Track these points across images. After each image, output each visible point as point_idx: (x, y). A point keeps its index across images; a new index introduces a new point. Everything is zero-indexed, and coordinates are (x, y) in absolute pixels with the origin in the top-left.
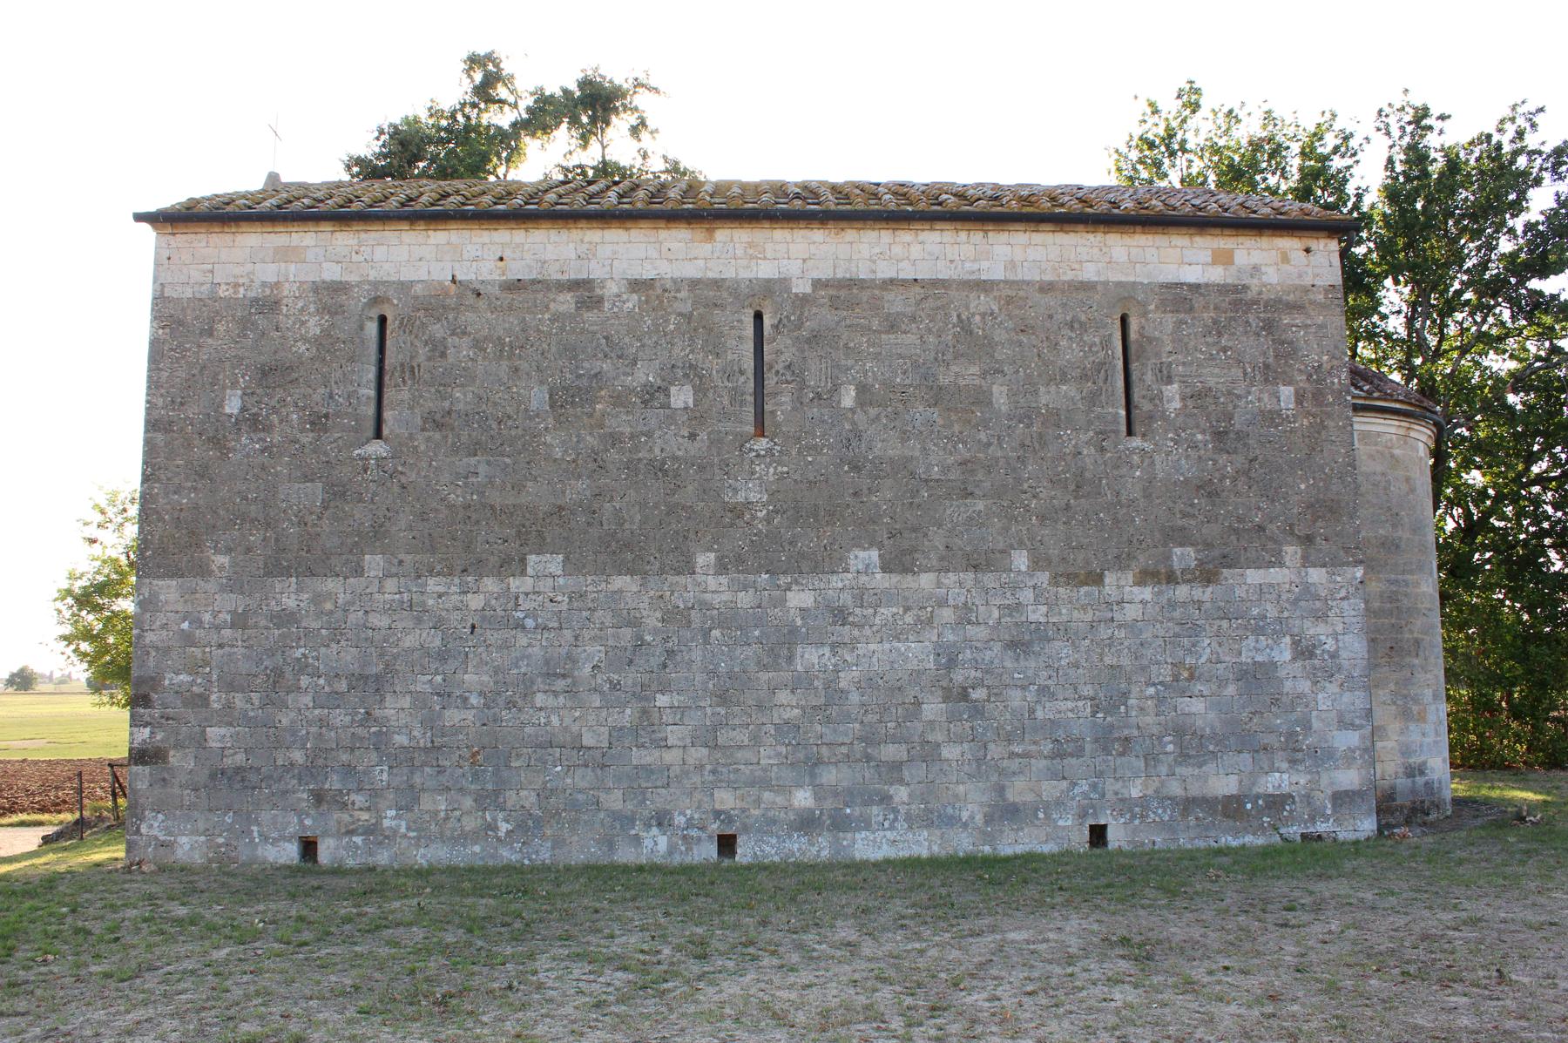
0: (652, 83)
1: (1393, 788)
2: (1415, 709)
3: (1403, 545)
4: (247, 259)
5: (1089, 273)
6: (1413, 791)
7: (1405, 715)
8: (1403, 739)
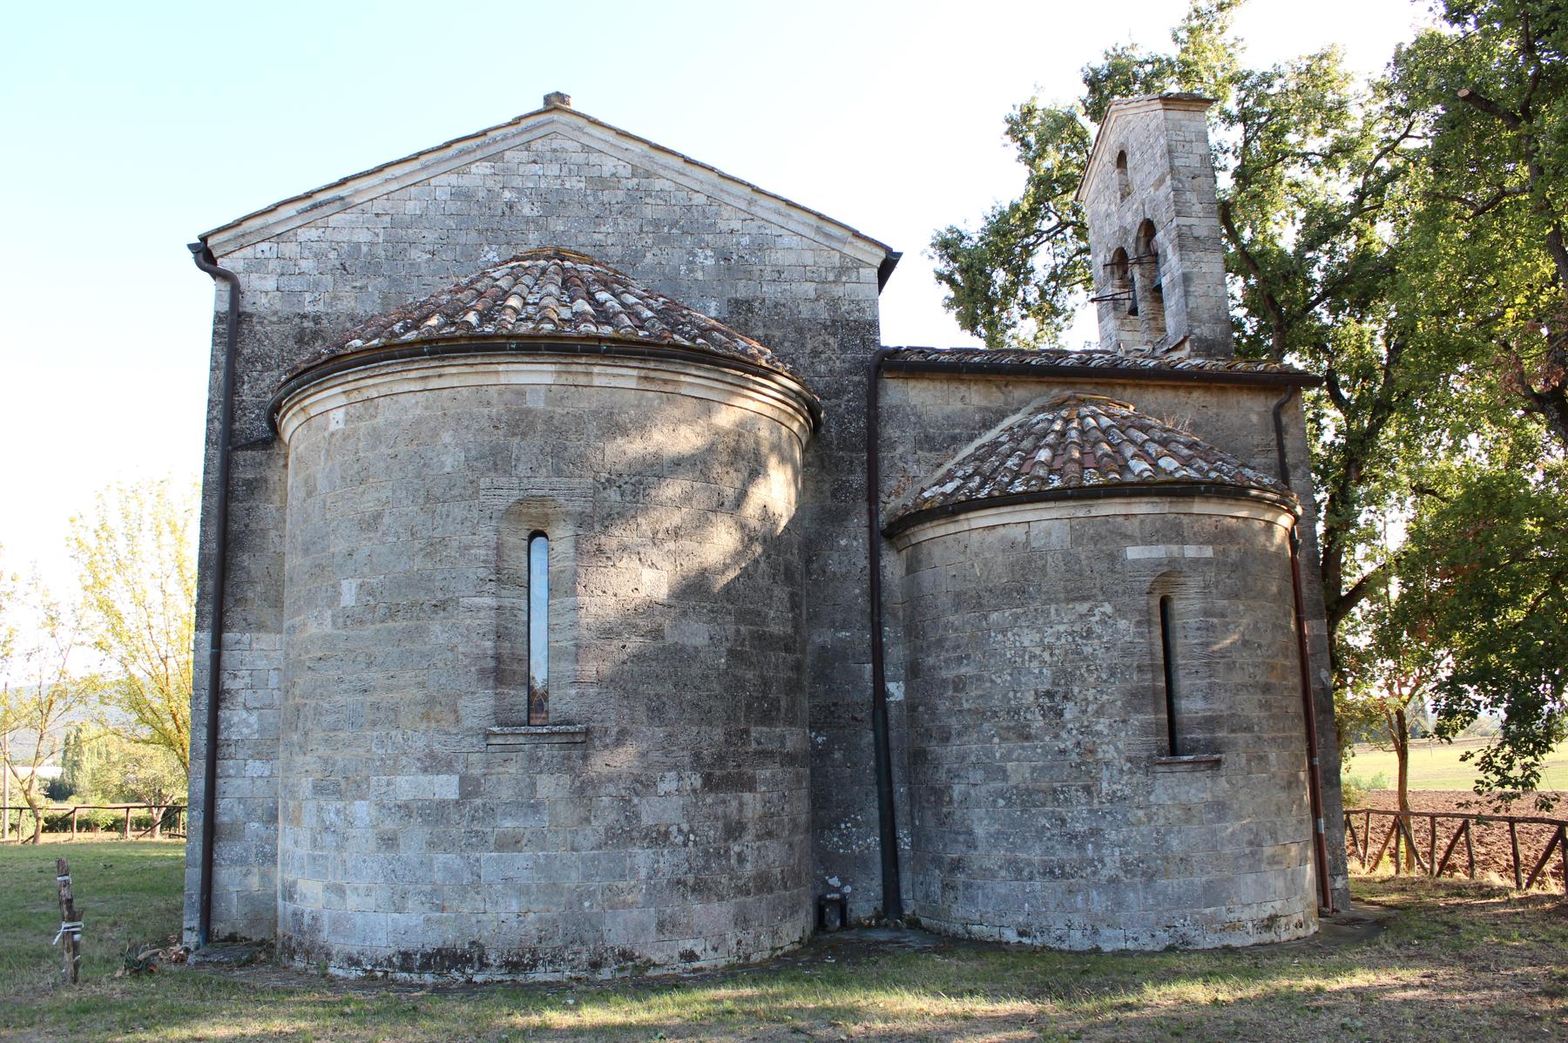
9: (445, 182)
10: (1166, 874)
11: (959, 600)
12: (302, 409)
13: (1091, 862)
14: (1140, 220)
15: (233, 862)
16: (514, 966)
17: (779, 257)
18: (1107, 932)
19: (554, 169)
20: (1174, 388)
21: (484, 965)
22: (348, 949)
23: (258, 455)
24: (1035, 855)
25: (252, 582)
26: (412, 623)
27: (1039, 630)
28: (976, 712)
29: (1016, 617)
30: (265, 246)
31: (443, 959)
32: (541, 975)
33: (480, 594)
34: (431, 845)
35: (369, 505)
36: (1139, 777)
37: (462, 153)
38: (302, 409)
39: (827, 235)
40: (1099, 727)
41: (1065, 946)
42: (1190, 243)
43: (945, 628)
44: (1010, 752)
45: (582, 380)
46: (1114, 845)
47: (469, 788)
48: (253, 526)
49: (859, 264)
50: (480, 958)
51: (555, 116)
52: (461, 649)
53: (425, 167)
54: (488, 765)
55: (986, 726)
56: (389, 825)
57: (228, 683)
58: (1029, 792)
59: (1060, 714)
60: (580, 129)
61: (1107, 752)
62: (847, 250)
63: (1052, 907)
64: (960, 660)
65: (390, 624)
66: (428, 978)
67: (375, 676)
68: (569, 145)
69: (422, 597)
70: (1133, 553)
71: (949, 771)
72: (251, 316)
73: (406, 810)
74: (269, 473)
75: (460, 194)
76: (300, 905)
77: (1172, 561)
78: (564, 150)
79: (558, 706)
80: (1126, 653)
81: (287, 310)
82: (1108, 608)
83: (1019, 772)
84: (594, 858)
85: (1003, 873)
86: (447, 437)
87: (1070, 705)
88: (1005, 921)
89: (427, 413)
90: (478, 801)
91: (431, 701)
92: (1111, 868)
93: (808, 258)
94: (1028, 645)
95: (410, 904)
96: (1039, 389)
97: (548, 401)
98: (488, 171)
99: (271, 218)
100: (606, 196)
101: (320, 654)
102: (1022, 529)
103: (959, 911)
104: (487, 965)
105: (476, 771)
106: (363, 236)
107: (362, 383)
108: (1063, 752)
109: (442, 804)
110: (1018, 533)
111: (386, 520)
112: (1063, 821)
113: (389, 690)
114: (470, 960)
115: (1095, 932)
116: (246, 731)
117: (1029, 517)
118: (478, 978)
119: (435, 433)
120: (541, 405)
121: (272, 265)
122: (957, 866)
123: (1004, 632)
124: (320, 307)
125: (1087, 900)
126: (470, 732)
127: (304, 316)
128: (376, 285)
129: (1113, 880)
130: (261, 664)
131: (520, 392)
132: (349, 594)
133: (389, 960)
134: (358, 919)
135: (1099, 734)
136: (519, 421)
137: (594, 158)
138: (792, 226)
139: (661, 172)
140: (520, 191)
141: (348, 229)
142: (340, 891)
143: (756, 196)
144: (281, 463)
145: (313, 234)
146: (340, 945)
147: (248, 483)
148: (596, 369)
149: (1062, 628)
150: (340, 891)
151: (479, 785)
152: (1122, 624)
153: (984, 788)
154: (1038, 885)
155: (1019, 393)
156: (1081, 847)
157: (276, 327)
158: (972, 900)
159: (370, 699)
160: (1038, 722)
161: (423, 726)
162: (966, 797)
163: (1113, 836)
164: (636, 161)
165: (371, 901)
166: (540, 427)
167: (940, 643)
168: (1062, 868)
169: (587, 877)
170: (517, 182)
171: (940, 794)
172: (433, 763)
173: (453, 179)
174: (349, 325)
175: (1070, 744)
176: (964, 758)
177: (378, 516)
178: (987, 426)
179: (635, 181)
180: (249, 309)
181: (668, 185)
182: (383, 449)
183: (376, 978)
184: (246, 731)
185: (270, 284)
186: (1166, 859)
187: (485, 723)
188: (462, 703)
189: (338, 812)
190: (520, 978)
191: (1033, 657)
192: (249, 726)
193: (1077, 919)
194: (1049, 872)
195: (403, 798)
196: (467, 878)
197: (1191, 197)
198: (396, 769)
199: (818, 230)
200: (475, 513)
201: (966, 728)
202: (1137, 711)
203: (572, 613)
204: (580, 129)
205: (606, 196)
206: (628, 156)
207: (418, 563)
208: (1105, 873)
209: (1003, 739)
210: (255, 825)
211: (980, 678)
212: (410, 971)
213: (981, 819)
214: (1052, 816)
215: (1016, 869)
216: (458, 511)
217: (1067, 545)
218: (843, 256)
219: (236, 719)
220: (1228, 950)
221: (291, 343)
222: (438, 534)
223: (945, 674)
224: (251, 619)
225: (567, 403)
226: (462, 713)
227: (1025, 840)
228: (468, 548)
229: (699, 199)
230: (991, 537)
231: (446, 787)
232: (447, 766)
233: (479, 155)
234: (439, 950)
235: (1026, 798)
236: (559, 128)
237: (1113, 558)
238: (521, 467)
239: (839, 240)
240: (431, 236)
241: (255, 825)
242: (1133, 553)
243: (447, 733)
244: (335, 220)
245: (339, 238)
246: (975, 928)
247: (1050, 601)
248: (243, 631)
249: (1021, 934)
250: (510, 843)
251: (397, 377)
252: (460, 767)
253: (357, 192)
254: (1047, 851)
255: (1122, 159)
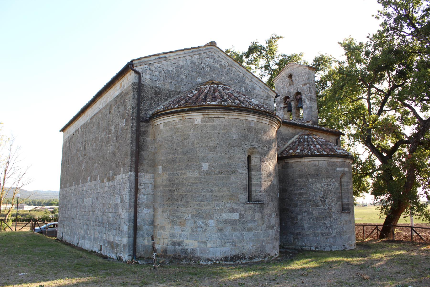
0: (339, 45)
1: (166, 248)
2: (178, 221)
3: (177, 160)
4: (72, 130)
5: (101, 107)
6: (175, 251)
7: (173, 223)
8: (171, 231)
9: (189, 58)
10: (343, 235)
11: (301, 176)
12: (183, 116)
13: (330, 232)
14: (296, 91)
15: (141, 237)
16: (251, 258)
17: (256, 92)
18: (333, 247)
19: (212, 60)
20: (322, 133)
21: (245, 259)
22: (207, 257)
23: (146, 124)
24: (319, 231)
25: (145, 159)
26: (226, 176)
27: (321, 184)
28: (305, 200)
29: (316, 181)
30: (146, 66)
31: (236, 258)
32: (256, 260)
33: (243, 170)
34: (233, 230)
35: (212, 145)
36: (339, 215)
37: (194, 52)
38: (183, 116)
39: (266, 89)
40: (332, 205)
41: (325, 250)
42: (312, 99)
43: (297, 182)
44: (314, 209)
45: (261, 121)
46: (335, 229)
47: (241, 216)
48: (145, 144)
49: (271, 96)
50: (244, 257)
51: (213, 47)
52: (239, 183)
53: (185, 53)
54: (246, 211)
55: (308, 204)
56: (221, 226)
57: (139, 187)
58: (318, 218)
59: (325, 201)
60: (218, 52)
61: (334, 210)
62: (269, 93)
63: (323, 242)
64: (301, 189)
65: (220, 175)
66: (232, 263)
67: (215, 188)
68: (215, 55)
69: (229, 169)
70: (338, 169)
71: (297, 213)
72: (143, 85)
73: (225, 222)
74: (148, 130)
75: (192, 62)
76: (185, 247)
77: (344, 171)
78: (214, 56)
79: (255, 197)
80: (337, 189)
81: (152, 85)
82: (334, 180)
83: (316, 214)
84: (265, 233)
85: (312, 235)
86: (234, 130)
87: (327, 200)
88: (312, 245)
89: (228, 124)
90: (244, 220)
91: (232, 195)
92: (334, 234)
93: (262, 93)
94: (318, 187)
95: (227, 245)
96: (301, 130)
97: (255, 125)
98: (198, 58)
99: (149, 59)
100: (223, 70)
101: (193, 182)
102: (317, 162)
103: (299, 244)
104: (246, 259)
105: (243, 212)
106: (170, 69)
107: (210, 113)
108: (325, 209)
109: (235, 220)
110: (316, 163)
111: (218, 149)
112: (325, 224)
113: (220, 192)
114: (242, 258)
115: (331, 247)
116: (143, 200)
117: (319, 160)
118: (244, 262)
119: (231, 129)
120: (254, 126)
121: (148, 72)
122: (298, 234)
123: (313, 184)
124: (160, 86)
125: (330, 240)
126: (241, 203)
127: (156, 88)
128: (174, 82)
129: (335, 236)
130: (147, 182)
131: (249, 122)
132: (205, 167)
133: (221, 259)
134: (211, 250)
135: (332, 206)
136: (250, 129)
137: (221, 60)
138: (259, 85)
139: (234, 66)
140: (205, 64)
141: (166, 66)
142: (205, 243)
143: (253, 77)
144: (151, 127)
145: (158, 65)
146: (203, 256)
147: (143, 131)
148: (264, 119)
149: (325, 184)
150: (205, 243)
151: (244, 216)
152: (336, 183)
153: (307, 217)
154: (320, 237)
155: (298, 130)
156: (329, 229)
157: (150, 89)
158: (303, 241)
159: (213, 194)
160: (320, 203)
161: (230, 201)
162: (302, 219)
163: (334, 227)
164: (229, 62)
165: (215, 245)
166: (253, 131)
167: (295, 185)
168: (325, 234)
169: (264, 237)
170: (204, 62)
171: (293, 219)
172: (232, 210)
173: (190, 58)
174: (167, 92)
175: (327, 208)
176: (301, 210)
177: (215, 148)
178: (293, 137)
179: (229, 67)
180: (143, 83)
181: (235, 70)
182: (216, 131)
183: (217, 264)
184: (143, 200)
185: (148, 77)
186: (343, 232)
187: (245, 201)
188: (240, 196)
189: (203, 223)
190: (252, 261)
191: (319, 189)
192: (144, 199)
193: (328, 244)
194: (322, 235)
195: (224, 219)
196: (241, 238)
197: (312, 89)
198: (222, 212)
199: (264, 87)
200: (241, 150)
201: (302, 204)
202: (339, 201)
203: (259, 176)
204: (218, 52)
205: (223, 70)
206: (228, 61)
207: (227, 161)
208: (333, 234)
209: (312, 206)
210: (146, 226)
211: (306, 193)
212: (227, 261)
213: (306, 224)
214: (323, 223)
215: (315, 234)
216: (237, 149)
217: (326, 166)
218: (268, 94)
219: (141, 197)
220: (351, 249)
221: (153, 94)
222: (232, 154)
223: (296, 192)
224: (144, 169)
225: (258, 126)
226: (239, 198)
227: (317, 228)
228: (240, 158)
229: (241, 75)
230: (310, 163)
231: (236, 216)
232: (236, 211)
233: (196, 53)
234: (235, 256)
235: (317, 219)
236: (214, 50)
237: (335, 170)
238: (250, 140)
239: (268, 90)
240: (186, 72)
241: (146, 226)
242: (338, 169)
243: (236, 203)
244: (164, 62)
245: (165, 68)
246: (304, 247)
247: (323, 178)
248: (142, 173)
249: (316, 248)
250: (250, 230)
251: (222, 113)
252: (239, 211)
253: (170, 56)
254: (322, 230)
255: (290, 76)
